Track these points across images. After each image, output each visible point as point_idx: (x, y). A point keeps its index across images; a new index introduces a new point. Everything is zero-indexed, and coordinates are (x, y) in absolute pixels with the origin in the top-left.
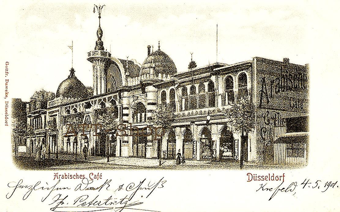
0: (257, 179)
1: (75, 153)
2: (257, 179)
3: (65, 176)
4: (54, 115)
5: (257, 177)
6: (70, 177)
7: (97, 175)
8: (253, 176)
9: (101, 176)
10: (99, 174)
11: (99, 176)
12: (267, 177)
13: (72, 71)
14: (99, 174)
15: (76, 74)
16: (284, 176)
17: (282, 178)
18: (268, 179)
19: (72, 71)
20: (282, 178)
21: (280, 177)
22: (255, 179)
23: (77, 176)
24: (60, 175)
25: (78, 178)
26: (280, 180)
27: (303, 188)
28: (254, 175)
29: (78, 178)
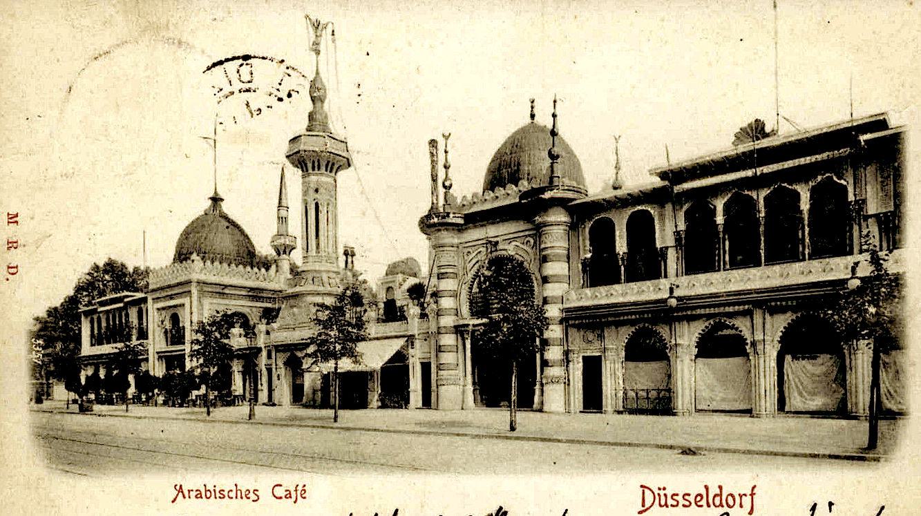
0: (670, 502)
1: (535, 232)
2: (670, 502)
3: (206, 491)
4: (175, 306)
5: (669, 497)
6: (218, 495)
7: (292, 489)
8: (656, 492)
9: (303, 492)
10: (300, 488)
11: (299, 492)
12: (699, 498)
13: (216, 200)
14: (300, 488)
15: (226, 207)
16: (752, 495)
17: (747, 501)
18: (704, 502)
19: (216, 200)
20: (747, 501)
21: (189, 491)
22: (663, 503)
23: (239, 492)
24: (192, 490)
25: (242, 498)
26: (741, 506)
27: (567, 510)
28: (659, 489)
29: (242, 498)
